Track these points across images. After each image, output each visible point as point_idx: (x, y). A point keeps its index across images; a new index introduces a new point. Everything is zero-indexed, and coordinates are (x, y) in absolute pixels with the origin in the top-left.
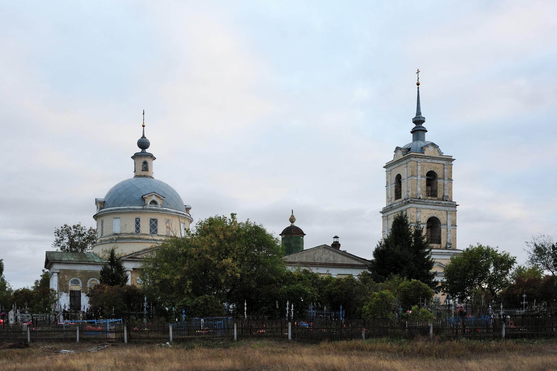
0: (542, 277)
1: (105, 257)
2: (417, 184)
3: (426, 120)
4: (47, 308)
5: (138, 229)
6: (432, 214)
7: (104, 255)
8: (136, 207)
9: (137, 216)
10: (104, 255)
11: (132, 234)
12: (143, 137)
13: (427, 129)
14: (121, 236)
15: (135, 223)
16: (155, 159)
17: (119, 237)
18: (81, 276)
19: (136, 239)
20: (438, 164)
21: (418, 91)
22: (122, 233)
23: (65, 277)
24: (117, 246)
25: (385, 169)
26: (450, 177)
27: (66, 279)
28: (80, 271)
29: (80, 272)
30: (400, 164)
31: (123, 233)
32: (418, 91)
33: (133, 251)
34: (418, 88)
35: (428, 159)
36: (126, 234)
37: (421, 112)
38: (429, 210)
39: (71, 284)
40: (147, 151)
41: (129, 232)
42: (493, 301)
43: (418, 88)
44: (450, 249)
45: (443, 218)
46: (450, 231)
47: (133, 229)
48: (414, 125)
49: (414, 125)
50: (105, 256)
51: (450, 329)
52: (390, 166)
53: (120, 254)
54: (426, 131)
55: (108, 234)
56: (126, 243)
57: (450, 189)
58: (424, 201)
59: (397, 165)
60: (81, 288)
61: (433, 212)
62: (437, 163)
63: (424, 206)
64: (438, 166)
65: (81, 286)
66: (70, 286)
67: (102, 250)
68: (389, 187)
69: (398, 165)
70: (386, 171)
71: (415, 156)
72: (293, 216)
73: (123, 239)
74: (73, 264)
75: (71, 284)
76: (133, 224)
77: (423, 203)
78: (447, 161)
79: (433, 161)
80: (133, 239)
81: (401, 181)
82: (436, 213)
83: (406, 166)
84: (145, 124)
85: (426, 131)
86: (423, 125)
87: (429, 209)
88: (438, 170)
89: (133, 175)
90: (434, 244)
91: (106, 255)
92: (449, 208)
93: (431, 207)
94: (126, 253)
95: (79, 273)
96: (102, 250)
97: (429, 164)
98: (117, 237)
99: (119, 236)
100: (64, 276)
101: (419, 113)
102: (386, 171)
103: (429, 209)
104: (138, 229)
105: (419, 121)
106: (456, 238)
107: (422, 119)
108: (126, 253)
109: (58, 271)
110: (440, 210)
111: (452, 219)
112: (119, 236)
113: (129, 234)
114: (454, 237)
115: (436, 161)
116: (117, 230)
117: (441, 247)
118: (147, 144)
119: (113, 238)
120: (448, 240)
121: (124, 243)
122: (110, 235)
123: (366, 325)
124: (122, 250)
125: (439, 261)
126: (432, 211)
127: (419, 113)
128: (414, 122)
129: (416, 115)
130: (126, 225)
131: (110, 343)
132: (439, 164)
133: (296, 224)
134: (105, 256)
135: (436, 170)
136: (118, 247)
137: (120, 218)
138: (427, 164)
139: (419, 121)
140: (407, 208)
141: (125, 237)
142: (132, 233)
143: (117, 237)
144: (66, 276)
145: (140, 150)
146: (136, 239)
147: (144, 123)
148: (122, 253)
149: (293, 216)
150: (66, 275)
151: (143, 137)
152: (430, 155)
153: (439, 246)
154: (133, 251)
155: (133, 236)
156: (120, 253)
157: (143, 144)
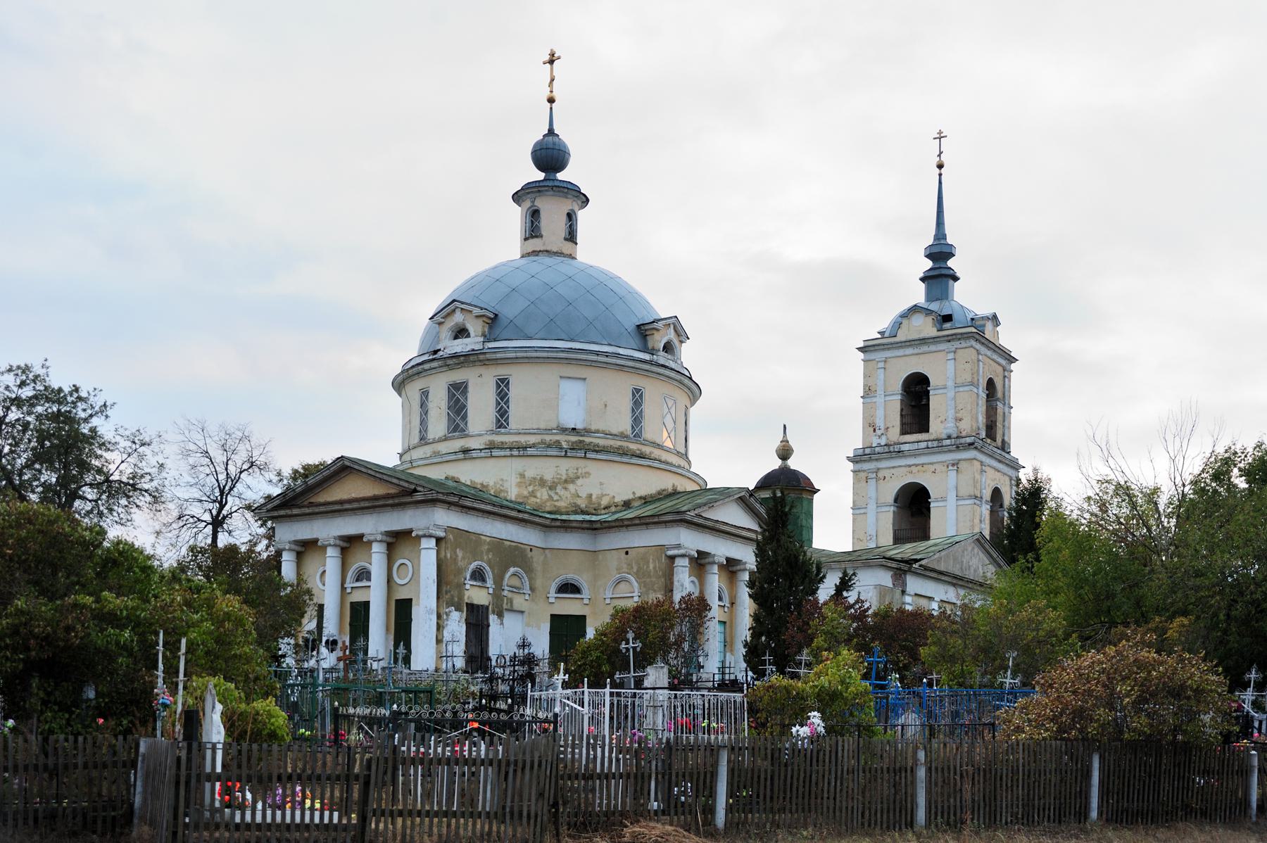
0: (490, 557)
1: (533, 499)
2: (978, 405)
3: (957, 252)
5: (637, 420)
7: (533, 494)
10: (533, 494)
11: (623, 436)
12: (551, 132)
13: (958, 274)
14: (587, 440)
15: (495, 396)
17: (581, 442)
18: (490, 557)
19: (634, 455)
21: (940, 183)
22: (593, 428)
23: (457, 556)
24: (587, 470)
25: (861, 355)
27: (460, 563)
28: (488, 539)
29: (489, 543)
30: (925, 348)
31: (597, 431)
32: (940, 183)
33: (634, 493)
34: (940, 175)
36: (603, 432)
37: (946, 232)
39: (556, 595)
40: (561, 176)
41: (614, 431)
42: (763, 638)
43: (940, 175)
47: (625, 425)
48: (929, 264)
49: (929, 264)
50: (535, 497)
52: (883, 349)
53: (594, 497)
54: (956, 279)
55: (536, 427)
56: (616, 465)
58: (930, 443)
59: (909, 351)
60: (490, 596)
65: (491, 591)
66: (468, 587)
67: (522, 476)
68: (880, 400)
69: (916, 351)
70: (862, 360)
71: (946, 338)
72: (785, 441)
73: (598, 450)
74: (503, 519)
75: (556, 595)
76: (627, 404)
80: (623, 453)
81: (928, 392)
83: (951, 356)
84: (555, 94)
85: (956, 279)
86: (950, 263)
91: (539, 495)
94: (614, 497)
95: (486, 547)
96: (522, 476)
98: (574, 438)
99: (581, 438)
100: (455, 553)
101: (940, 233)
102: (862, 360)
104: (637, 420)
105: (940, 253)
107: (946, 250)
108: (614, 497)
109: (441, 534)
112: (581, 438)
113: (615, 435)
116: (572, 416)
118: (555, 152)
119: (558, 442)
121: (611, 464)
122: (548, 431)
123: (1112, 762)
124: (601, 484)
127: (940, 233)
129: (935, 240)
130: (606, 405)
131: (321, 724)
133: (793, 463)
134: (535, 497)
136: (588, 474)
137: (585, 379)
139: (940, 253)
140: (959, 460)
141: (602, 442)
142: (622, 433)
143: (574, 438)
144: (460, 553)
145: (540, 176)
146: (634, 455)
147: (551, 92)
148: (603, 495)
149: (785, 441)
150: (462, 549)
151: (551, 132)
154: (634, 493)
155: (625, 444)
156: (596, 493)
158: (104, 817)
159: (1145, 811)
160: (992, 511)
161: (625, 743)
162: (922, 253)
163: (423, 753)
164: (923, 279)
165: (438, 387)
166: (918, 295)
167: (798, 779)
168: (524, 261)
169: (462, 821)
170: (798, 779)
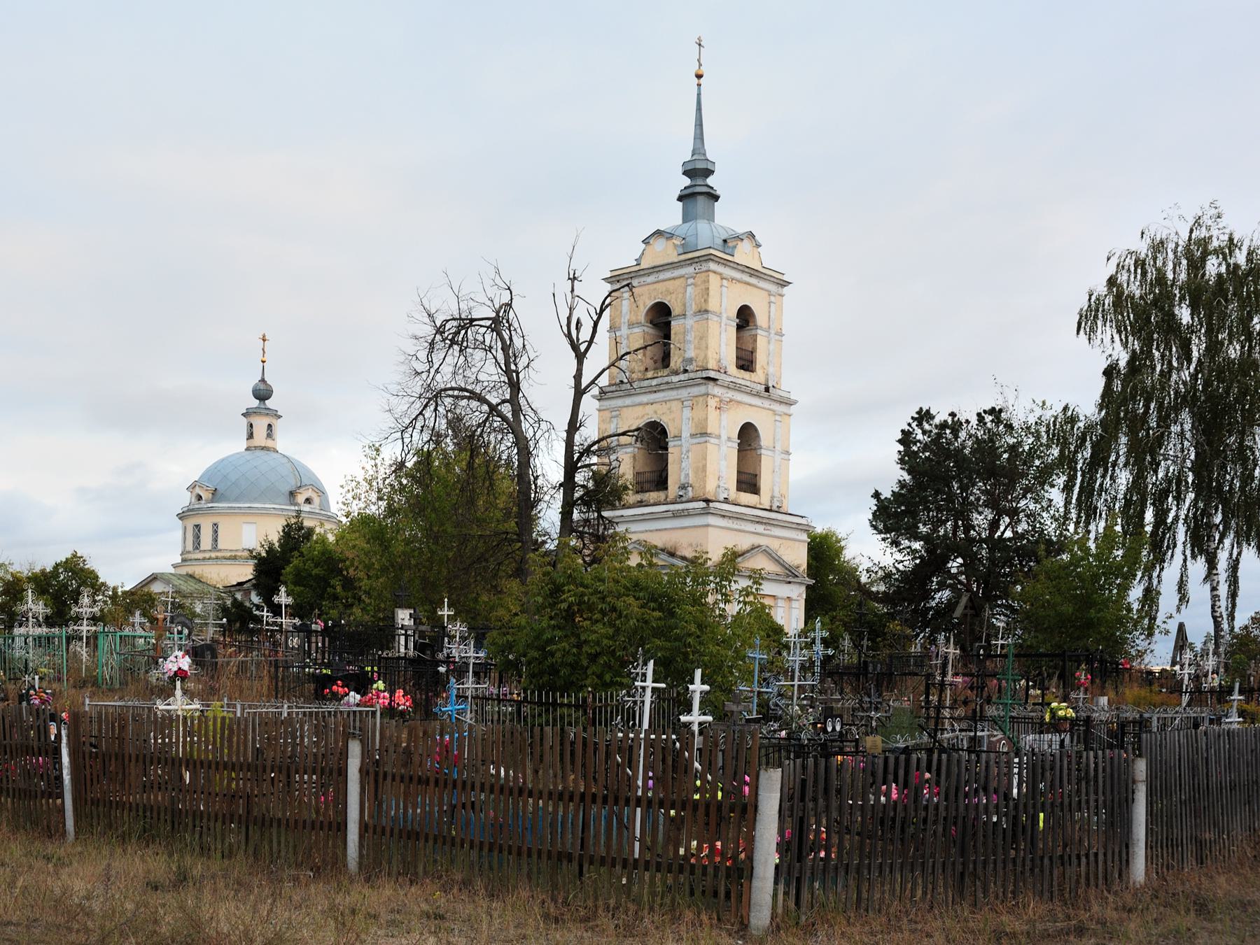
3: (717, 169)
4: (720, 798)
6: (646, 417)
8: (267, 506)
9: (215, 520)
12: (263, 380)
13: (718, 193)
16: (280, 417)
20: (672, 282)
21: (699, 95)
26: (703, 305)
32: (699, 95)
34: (699, 85)
35: (649, 274)
38: (641, 407)
40: (269, 403)
43: (699, 85)
44: (684, 499)
45: (674, 420)
46: (688, 451)
49: (687, 181)
51: (535, 703)
57: (701, 338)
61: (650, 409)
62: (670, 279)
63: (628, 401)
64: (670, 285)
77: (621, 393)
78: (694, 265)
79: (662, 276)
82: (656, 412)
86: (710, 181)
87: (640, 404)
88: (674, 296)
89: (242, 444)
90: (652, 493)
92: (689, 390)
93: (645, 398)
97: (651, 287)
103: (640, 404)
105: (698, 171)
106: (705, 466)
110: (666, 402)
111: (696, 420)
114: (701, 465)
115: (668, 275)
117: (667, 497)
120: (682, 478)
125: (642, 537)
126: (647, 407)
128: (686, 173)
132: (674, 279)
135: (669, 298)
138: (647, 287)
139: (698, 171)
145: (255, 403)
151: (263, 380)
152: (670, 261)
153: (660, 495)
157: (262, 394)
158: (645, 681)
159: (1092, 773)
160: (705, 482)
161: (222, 756)
162: (680, 170)
163: (632, 740)
164: (680, 199)
165: (190, 523)
166: (671, 215)
167: (1161, 771)
168: (249, 455)
169: (234, 759)
170: (1161, 771)
